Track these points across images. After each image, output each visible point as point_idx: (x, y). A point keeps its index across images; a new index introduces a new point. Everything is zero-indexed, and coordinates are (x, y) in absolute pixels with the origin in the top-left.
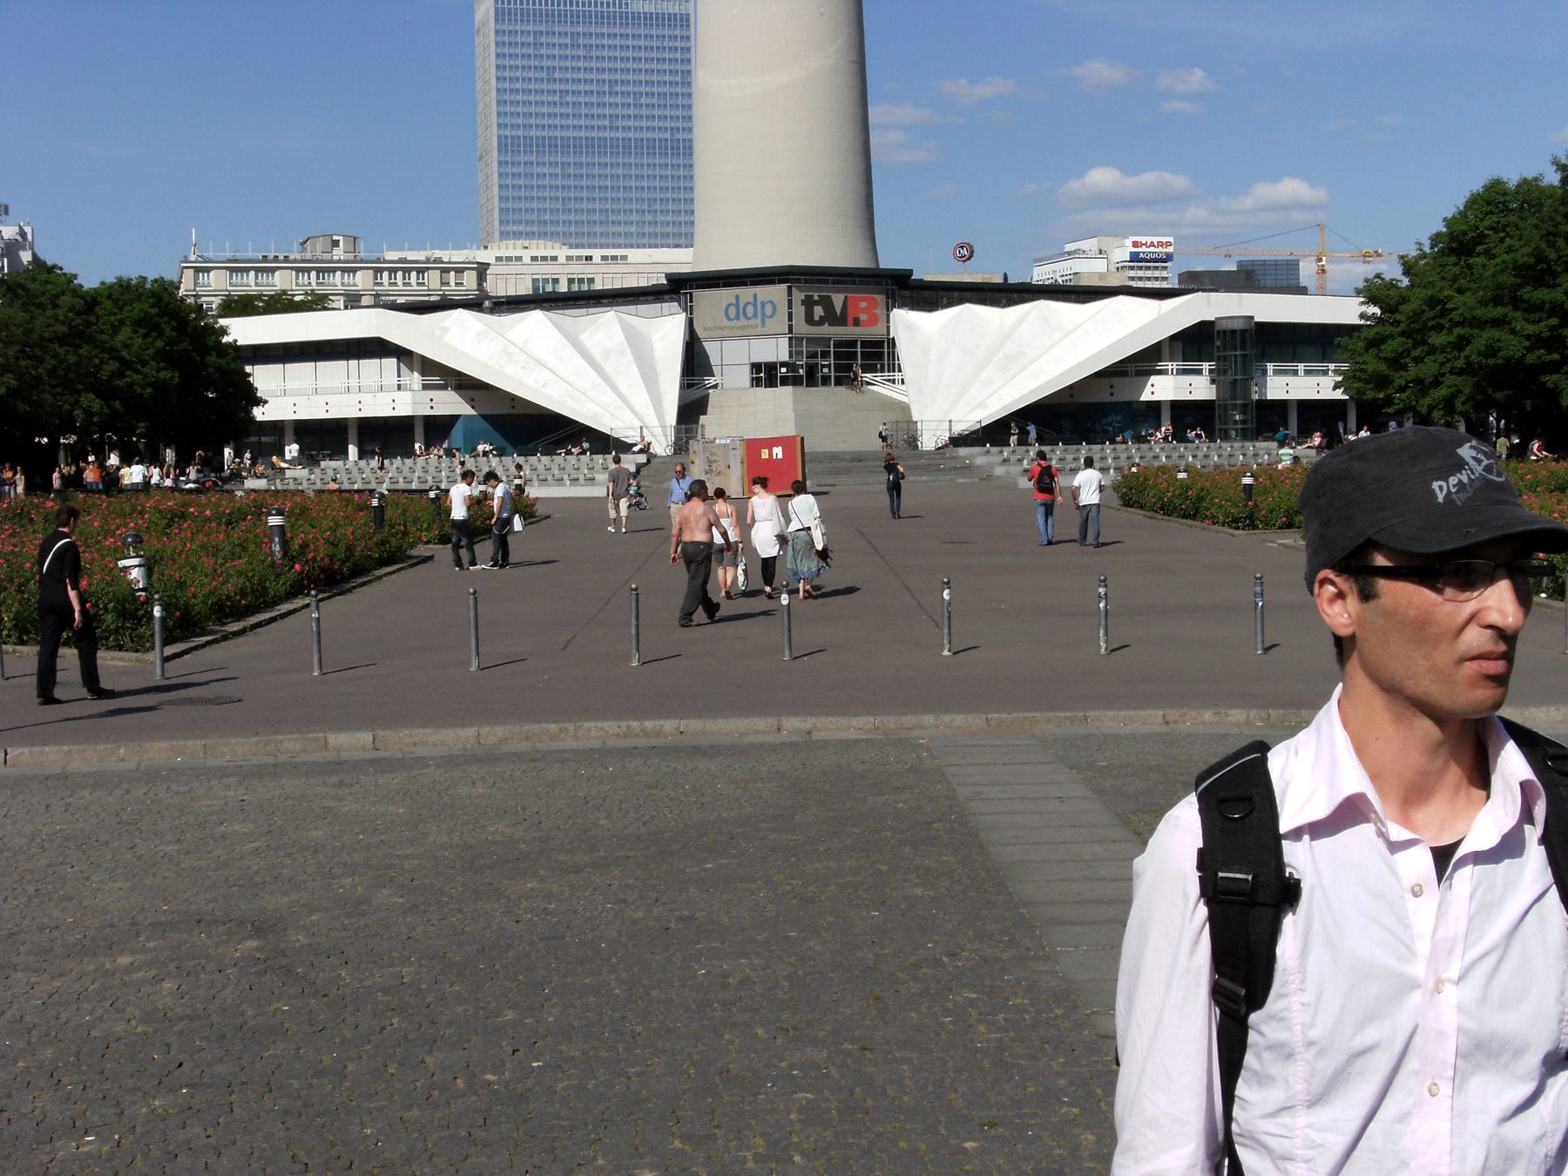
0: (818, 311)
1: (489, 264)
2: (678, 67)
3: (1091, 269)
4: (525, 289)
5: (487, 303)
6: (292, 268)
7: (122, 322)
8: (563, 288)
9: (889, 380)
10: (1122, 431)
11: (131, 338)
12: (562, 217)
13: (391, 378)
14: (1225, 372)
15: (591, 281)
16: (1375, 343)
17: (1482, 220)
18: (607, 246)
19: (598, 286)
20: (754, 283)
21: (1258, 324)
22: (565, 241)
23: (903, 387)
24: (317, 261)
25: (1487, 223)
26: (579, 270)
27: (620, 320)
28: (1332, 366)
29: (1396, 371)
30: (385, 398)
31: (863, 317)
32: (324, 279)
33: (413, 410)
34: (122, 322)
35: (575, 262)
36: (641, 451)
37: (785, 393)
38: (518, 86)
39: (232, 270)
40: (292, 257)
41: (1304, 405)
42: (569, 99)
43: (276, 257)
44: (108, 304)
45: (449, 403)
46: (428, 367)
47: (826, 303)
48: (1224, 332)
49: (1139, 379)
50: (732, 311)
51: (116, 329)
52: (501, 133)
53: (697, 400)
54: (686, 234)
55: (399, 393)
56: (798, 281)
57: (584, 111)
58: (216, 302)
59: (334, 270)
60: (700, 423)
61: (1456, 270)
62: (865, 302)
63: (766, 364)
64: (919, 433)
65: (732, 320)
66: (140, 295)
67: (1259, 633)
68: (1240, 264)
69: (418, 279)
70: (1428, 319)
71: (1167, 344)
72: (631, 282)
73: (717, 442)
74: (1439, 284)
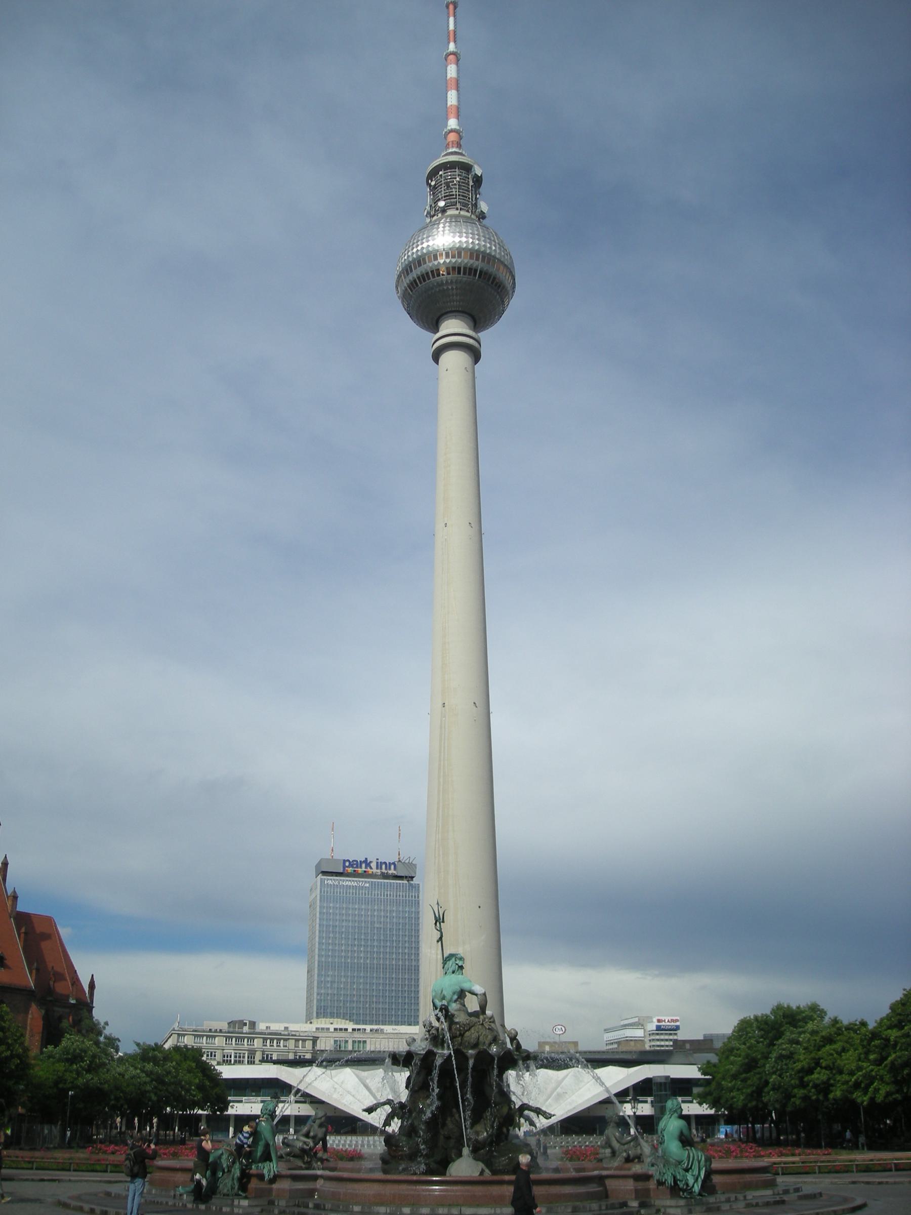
1: (318, 1037)
8: (350, 1048)
48: (657, 1083)
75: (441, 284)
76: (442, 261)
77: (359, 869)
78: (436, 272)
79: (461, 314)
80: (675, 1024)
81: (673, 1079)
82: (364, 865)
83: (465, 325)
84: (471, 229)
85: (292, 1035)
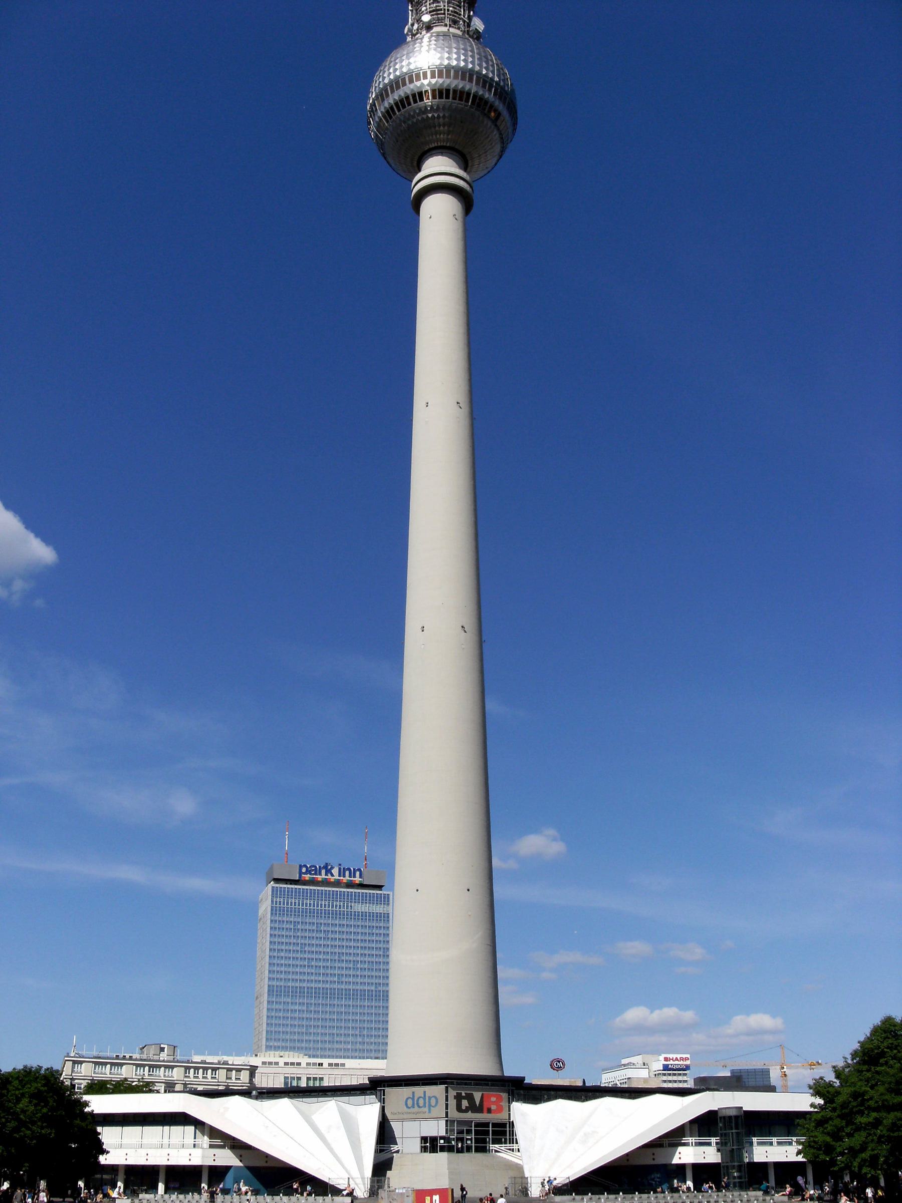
0: (465, 1103)
1: (257, 1067)
2: (381, 945)
3: (639, 1076)
4: (279, 1084)
5: (254, 1093)
6: (133, 1064)
7: (23, 1095)
8: (303, 1084)
9: (510, 1149)
10: (661, 1184)
11: (27, 1106)
12: (305, 1037)
13: (190, 1140)
14: (726, 1144)
15: (321, 1079)
16: (821, 1123)
17: (882, 1042)
18: (333, 1057)
19: (325, 1084)
20: (424, 1084)
21: (745, 1112)
22: (306, 1052)
24: (150, 1060)
25: (885, 1044)
26: (315, 1072)
27: (338, 1105)
28: (794, 1139)
29: (837, 1142)
30: (185, 1152)
31: (493, 1107)
32: (153, 1072)
33: (203, 1161)
34: (23, 1095)
35: (312, 1067)
36: (348, 1195)
37: (442, 1157)
38: (282, 954)
39: (96, 1063)
40: (134, 1057)
41: (778, 1165)
42: (313, 963)
43: (125, 1056)
44: (16, 1083)
45: (226, 1158)
46: (214, 1133)
47: (470, 1097)
48: (724, 1117)
49: (670, 1149)
50: (410, 1102)
51: (18, 1100)
52: (270, 983)
53: (386, 1160)
54: (383, 1051)
55: (194, 1149)
56: (452, 1083)
57: (322, 971)
58: (84, 1083)
59: (160, 1067)
60: (387, 1177)
61: (869, 1075)
62: (494, 1097)
63: (431, 1138)
64: (529, 1185)
65: (409, 1108)
66: (37, 1078)
68: (732, 1071)
69: (212, 1074)
70: (854, 1107)
71: (688, 1126)
72: (346, 1082)
73: (397, 1191)
74: (859, 1084)
75: (424, 111)
76: (426, 82)
77: (318, 876)
78: (419, 95)
79: (450, 151)
80: (685, 1063)
81: (746, 1112)
82: (323, 872)
83: (457, 165)
84: (462, 44)
85: (223, 1064)
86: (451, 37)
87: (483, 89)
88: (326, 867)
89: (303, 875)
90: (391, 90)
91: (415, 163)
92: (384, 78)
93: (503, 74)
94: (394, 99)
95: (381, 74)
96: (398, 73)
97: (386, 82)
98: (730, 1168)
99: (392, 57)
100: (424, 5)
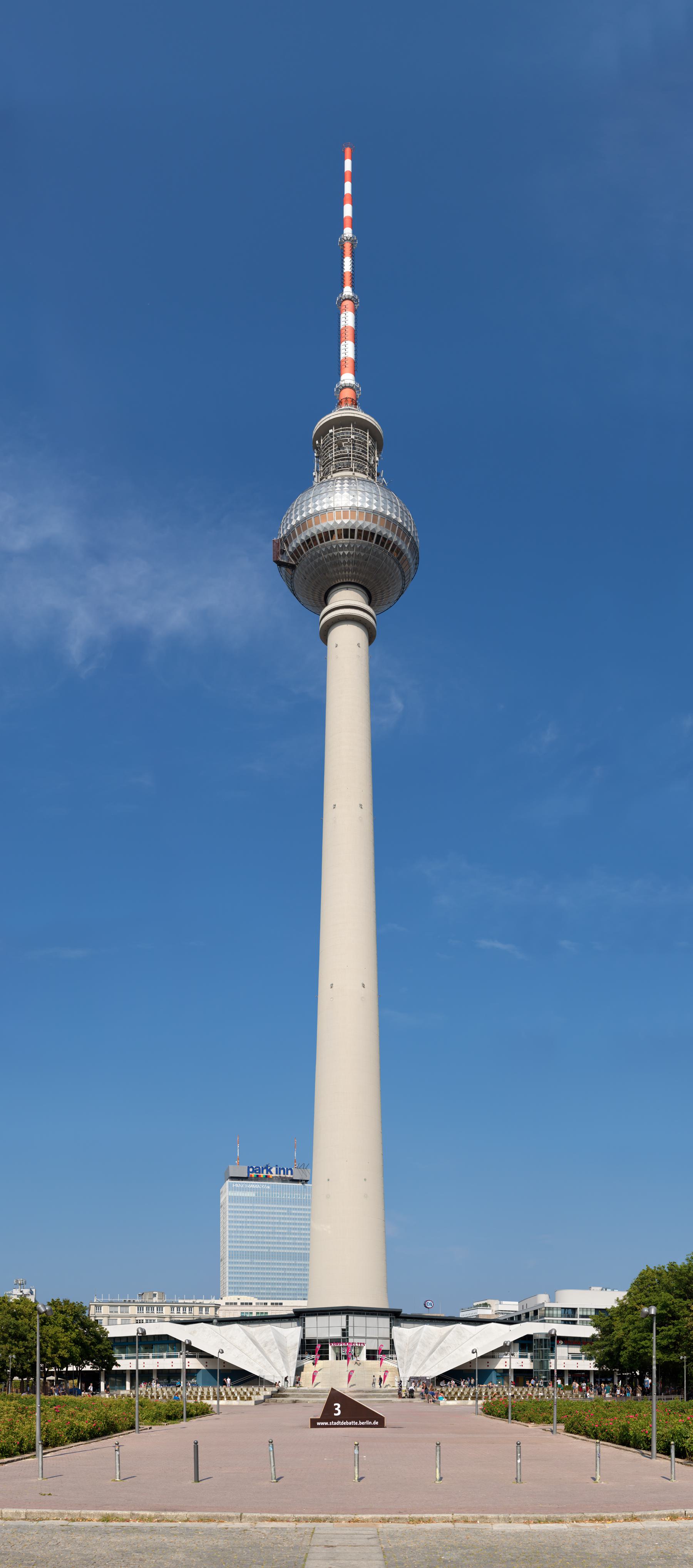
4: (237, 1315)
6: (136, 1305)
8: (254, 1315)
23: (396, 1361)
24: (147, 1303)
40: (136, 1301)
45: (194, 1364)
48: (537, 1340)
56: (351, 1313)
67: (438, 1459)
82: (265, 1171)
86: (356, 481)
87: (387, 530)
88: (266, 1168)
89: (250, 1174)
90: (298, 532)
91: (323, 599)
92: (291, 521)
93: (406, 517)
94: (302, 540)
95: (288, 517)
96: (310, 512)
97: (293, 524)
98: (539, 1373)
99: (298, 500)
100: (329, 451)
